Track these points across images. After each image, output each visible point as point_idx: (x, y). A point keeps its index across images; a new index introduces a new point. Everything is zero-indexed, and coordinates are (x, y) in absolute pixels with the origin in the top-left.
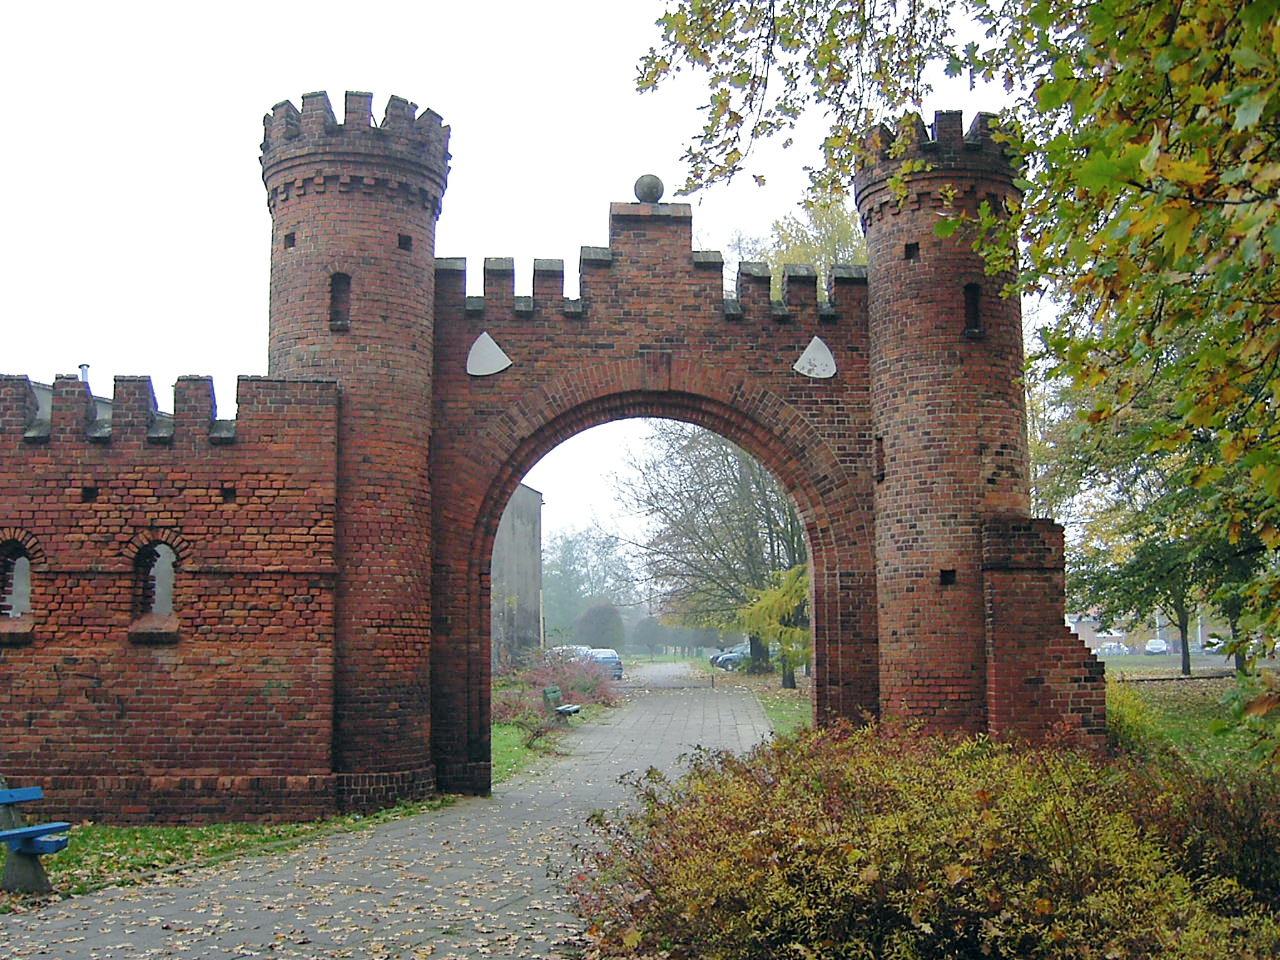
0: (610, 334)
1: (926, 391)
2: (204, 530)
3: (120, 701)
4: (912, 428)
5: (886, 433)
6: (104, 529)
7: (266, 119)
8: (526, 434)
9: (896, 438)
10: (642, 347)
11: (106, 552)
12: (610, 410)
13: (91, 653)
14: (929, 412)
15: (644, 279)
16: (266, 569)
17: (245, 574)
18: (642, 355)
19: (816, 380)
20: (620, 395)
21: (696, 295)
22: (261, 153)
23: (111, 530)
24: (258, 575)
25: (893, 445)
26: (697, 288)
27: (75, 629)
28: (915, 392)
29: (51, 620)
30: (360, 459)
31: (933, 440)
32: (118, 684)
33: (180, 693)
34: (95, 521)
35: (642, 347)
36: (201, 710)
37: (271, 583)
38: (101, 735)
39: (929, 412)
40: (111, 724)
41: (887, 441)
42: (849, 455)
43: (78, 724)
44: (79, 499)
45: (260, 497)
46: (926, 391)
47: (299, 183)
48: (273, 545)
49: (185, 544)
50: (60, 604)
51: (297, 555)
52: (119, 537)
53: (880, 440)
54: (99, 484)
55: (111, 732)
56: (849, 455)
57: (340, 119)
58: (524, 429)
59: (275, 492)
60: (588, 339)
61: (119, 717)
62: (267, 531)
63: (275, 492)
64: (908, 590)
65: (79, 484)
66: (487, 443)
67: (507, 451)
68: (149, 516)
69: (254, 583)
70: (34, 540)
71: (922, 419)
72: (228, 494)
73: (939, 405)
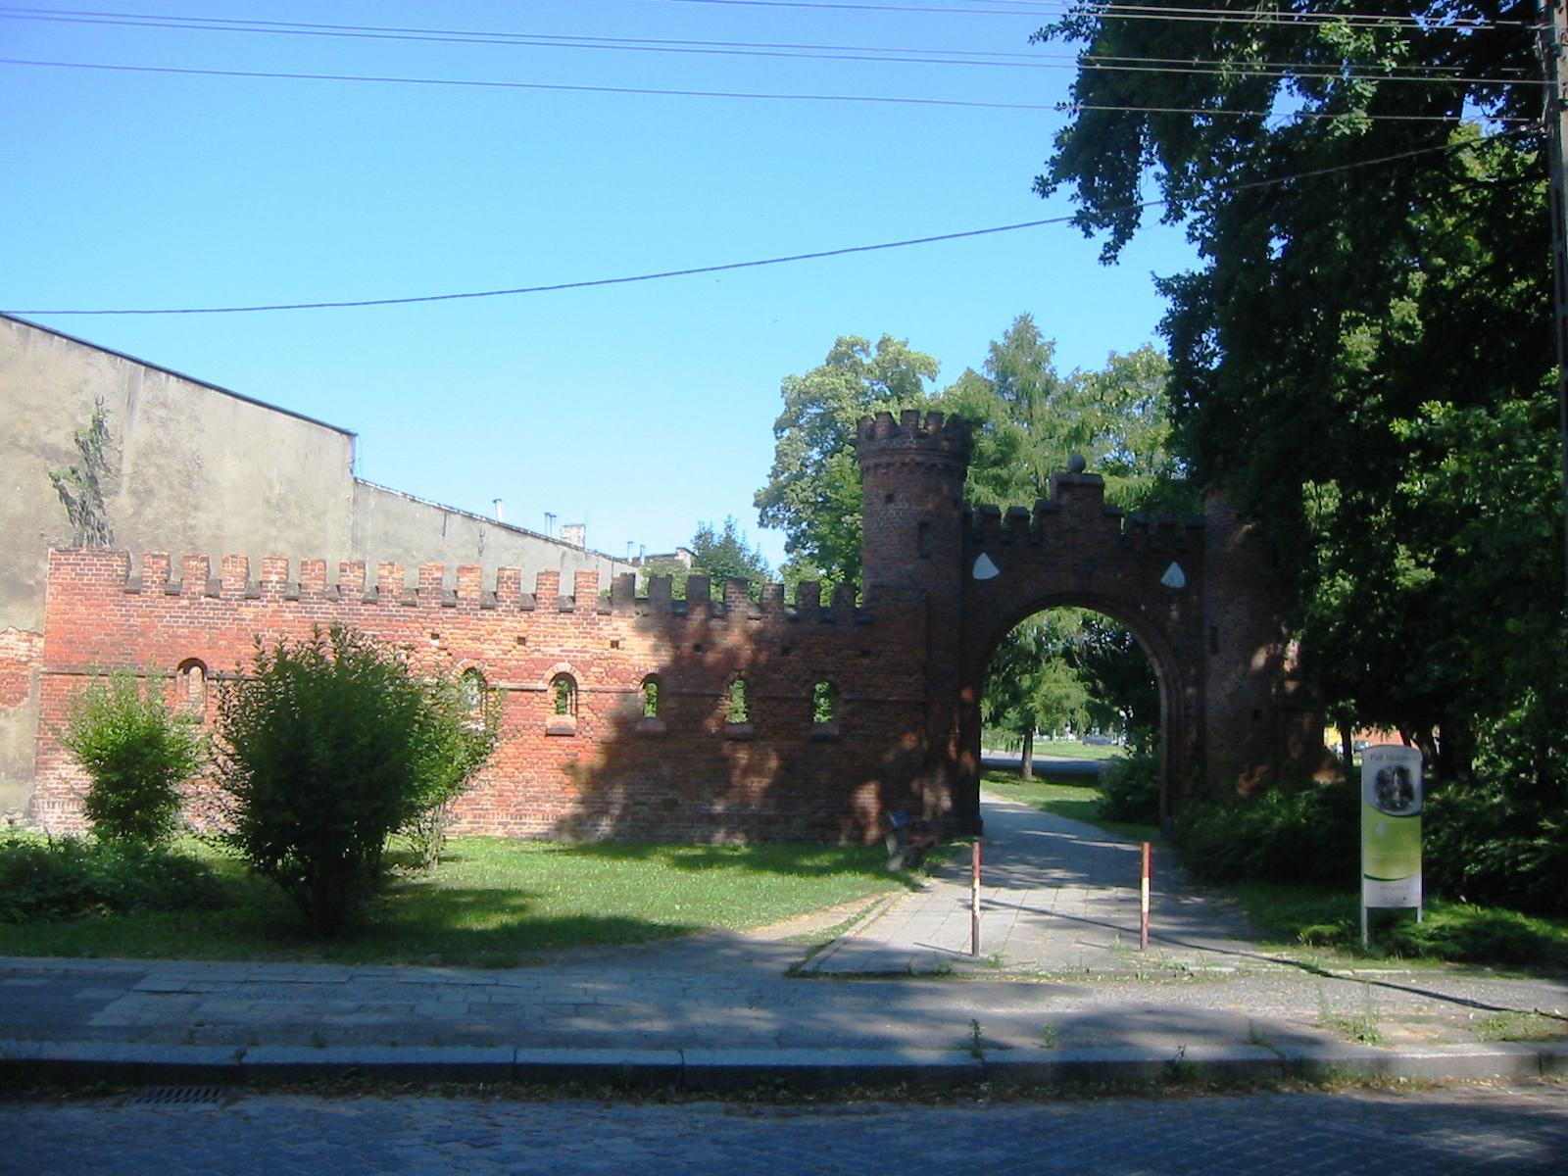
11: (796, 686)
16: (890, 699)
72: (865, 653)
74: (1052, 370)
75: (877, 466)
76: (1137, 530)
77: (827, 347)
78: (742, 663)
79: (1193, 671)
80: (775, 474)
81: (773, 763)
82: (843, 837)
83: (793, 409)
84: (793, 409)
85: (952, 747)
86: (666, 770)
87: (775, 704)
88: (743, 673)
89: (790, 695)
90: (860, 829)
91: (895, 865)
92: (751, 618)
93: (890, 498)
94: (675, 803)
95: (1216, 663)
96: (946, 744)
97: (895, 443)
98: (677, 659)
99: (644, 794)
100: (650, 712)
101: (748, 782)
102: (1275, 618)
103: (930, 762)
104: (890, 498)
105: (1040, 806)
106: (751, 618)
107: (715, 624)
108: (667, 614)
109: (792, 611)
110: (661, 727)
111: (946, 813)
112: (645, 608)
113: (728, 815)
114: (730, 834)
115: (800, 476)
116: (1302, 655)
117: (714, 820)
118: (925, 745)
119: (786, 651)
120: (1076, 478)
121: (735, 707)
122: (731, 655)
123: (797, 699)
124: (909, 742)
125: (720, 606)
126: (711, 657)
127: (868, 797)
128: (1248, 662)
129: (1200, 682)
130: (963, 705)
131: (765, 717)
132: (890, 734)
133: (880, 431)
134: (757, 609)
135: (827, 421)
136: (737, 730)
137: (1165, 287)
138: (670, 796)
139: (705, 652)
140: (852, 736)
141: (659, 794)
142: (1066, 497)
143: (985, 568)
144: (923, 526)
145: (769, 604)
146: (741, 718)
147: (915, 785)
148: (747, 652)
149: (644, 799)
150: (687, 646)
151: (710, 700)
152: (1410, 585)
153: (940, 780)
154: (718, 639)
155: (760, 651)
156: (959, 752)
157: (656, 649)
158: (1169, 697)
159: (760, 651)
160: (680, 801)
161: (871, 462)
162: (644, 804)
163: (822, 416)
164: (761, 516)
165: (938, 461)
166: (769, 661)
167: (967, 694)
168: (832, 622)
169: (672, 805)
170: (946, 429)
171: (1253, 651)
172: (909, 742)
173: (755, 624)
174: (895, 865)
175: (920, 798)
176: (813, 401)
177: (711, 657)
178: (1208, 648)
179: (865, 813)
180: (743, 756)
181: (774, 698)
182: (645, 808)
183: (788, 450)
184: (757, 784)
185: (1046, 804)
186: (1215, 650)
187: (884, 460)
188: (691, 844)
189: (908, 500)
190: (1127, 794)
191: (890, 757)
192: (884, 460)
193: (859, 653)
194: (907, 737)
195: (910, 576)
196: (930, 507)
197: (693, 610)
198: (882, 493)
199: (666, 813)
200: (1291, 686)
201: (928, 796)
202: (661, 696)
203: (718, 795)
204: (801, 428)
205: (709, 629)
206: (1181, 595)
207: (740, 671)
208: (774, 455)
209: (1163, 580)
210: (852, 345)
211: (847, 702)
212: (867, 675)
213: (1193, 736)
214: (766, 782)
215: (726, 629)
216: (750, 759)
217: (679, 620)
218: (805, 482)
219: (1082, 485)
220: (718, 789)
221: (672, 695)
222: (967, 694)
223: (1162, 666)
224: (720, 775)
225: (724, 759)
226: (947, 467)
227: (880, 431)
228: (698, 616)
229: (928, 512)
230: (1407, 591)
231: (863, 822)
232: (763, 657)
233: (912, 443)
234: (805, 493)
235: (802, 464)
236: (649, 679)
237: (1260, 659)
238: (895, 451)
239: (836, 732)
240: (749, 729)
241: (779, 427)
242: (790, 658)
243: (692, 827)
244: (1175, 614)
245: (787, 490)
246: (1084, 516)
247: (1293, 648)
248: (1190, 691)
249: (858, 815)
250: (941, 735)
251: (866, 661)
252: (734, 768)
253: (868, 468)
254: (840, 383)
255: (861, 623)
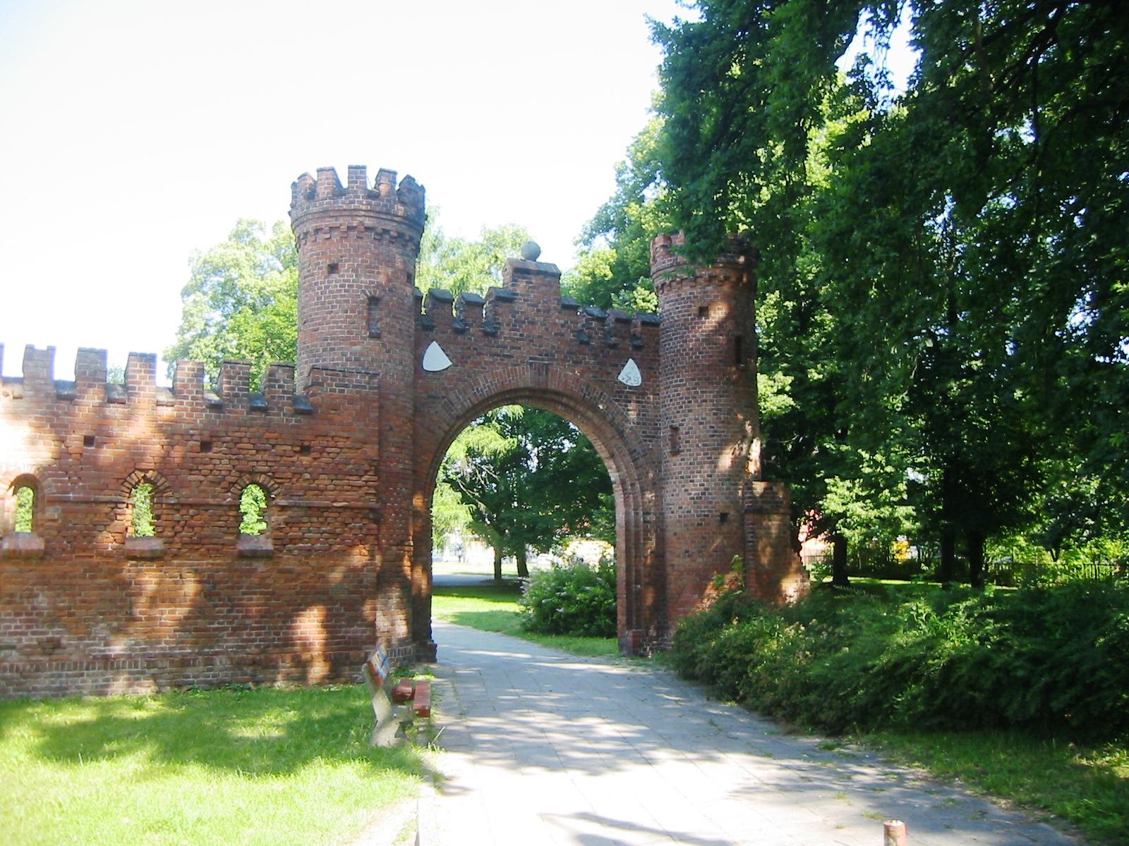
0: (512, 348)
1: (711, 401)
2: (289, 475)
3: (230, 600)
4: (702, 423)
5: (680, 425)
6: (217, 473)
7: (422, 188)
8: (461, 412)
9: (691, 428)
10: (531, 358)
11: (218, 489)
12: (510, 399)
13: (207, 564)
14: (714, 414)
15: (531, 313)
16: (335, 504)
17: (318, 508)
18: (531, 364)
19: (631, 387)
20: (516, 390)
21: (563, 326)
22: (290, 209)
23: (223, 473)
24: (327, 508)
25: (687, 433)
26: (562, 322)
27: (196, 547)
28: (705, 401)
29: (177, 539)
30: (388, 428)
31: (716, 432)
32: (228, 588)
33: (273, 593)
34: (210, 467)
35: (531, 358)
36: (288, 605)
37: (337, 514)
38: (216, 625)
39: (714, 414)
40: (223, 617)
41: (682, 430)
42: (648, 437)
43: (199, 618)
44: (199, 449)
45: (329, 453)
46: (711, 401)
47: (344, 228)
48: (338, 488)
49: (276, 486)
50: (183, 527)
51: (355, 495)
52: (230, 479)
53: (675, 429)
54: (214, 439)
55: (222, 623)
56: (648, 437)
57: (345, 184)
58: (458, 409)
59: (339, 450)
60: (498, 350)
61: (229, 611)
62: (333, 477)
63: (339, 450)
64: (698, 525)
65: (199, 438)
66: (435, 418)
67: (448, 425)
68: (250, 464)
69: (325, 514)
70: (163, 479)
71: (708, 418)
72: (305, 450)
73: (720, 410)
74: (439, 228)
75: (317, 230)
76: (594, 324)
77: (232, 227)
78: (150, 461)
79: (651, 475)
80: (182, 331)
81: (190, 587)
82: (279, 677)
83: (198, 277)
84: (198, 277)
85: (407, 563)
86: (43, 601)
87: (191, 512)
88: (150, 474)
89: (211, 501)
90: (302, 665)
91: (386, 737)
92: (158, 404)
93: (333, 268)
94: (56, 645)
95: (676, 465)
96: (401, 559)
97: (341, 203)
98: (61, 456)
99: (11, 634)
100: (24, 527)
101: (155, 612)
102: (740, 417)
103: (387, 578)
104: (333, 268)
105: (450, 619)
106: (158, 404)
107: (114, 411)
108: (48, 396)
109: (214, 398)
110: (38, 544)
111: (402, 642)
112: (17, 390)
113: (130, 656)
114: (134, 680)
115: (204, 334)
116: (764, 455)
117: (108, 663)
118: (378, 559)
119: (206, 446)
120: (531, 265)
121: (138, 518)
122: (134, 456)
123: (220, 505)
124: (359, 557)
125: (119, 388)
126: (107, 454)
127: (310, 626)
128: (714, 463)
129: (657, 485)
130: (416, 514)
131: (178, 528)
132: (336, 547)
133: (323, 191)
134: (171, 395)
135: (228, 288)
136: (141, 546)
137: (661, 33)
138: (50, 635)
139: (100, 445)
140: (290, 551)
141: (33, 633)
142: (522, 284)
143: (436, 359)
144: (373, 301)
145: (185, 386)
146: (146, 529)
147: (367, 609)
148: (155, 448)
149: (13, 640)
150: (75, 441)
151: (106, 509)
152: (775, 408)
153: (395, 600)
154: (116, 430)
155: (172, 445)
156: (412, 567)
157: (33, 442)
158: (626, 504)
159: (172, 445)
160: (64, 642)
161: (310, 227)
162: (13, 648)
163: (223, 285)
164: (168, 370)
165: (390, 226)
166: (184, 457)
167: (418, 502)
168: (264, 410)
169: (54, 645)
170: (399, 192)
171: (719, 450)
172: (359, 557)
173: (167, 412)
174: (386, 737)
175: (373, 625)
176: (217, 271)
177: (107, 454)
178: (667, 450)
179: (306, 647)
180: (150, 579)
181: (191, 506)
182: (14, 653)
183: (194, 311)
184: (170, 616)
185: (455, 616)
186: (675, 452)
187: (326, 223)
188: (78, 701)
189: (355, 270)
190: (559, 606)
191: (336, 575)
192: (326, 223)
193: (298, 449)
194: (356, 551)
195: (356, 360)
196: (382, 279)
197: (85, 392)
198: (324, 263)
199: (45, 659)
200: (759, 487)
201: (382, 623)
202: (37, 505)
203: (118, 631)
204: (205, 294)
205: (105, 417)
206: (639, 392)
207: (146, 471)
208: (182, 315)
209: (620, 378)
210: (251, 224)
211: (283, 508)
212: (308, 476)
213: (652, 544)
214: (181, 612)
215: (128, 417)
216: (159, 584)
217: (64, 404)
218: (208, 340)
219: (538, 273)
220: (115, 624)
221: (52, 502)
222: (418, 502)
223: (618, 469)
224: (119, 605)
225: (125, 585)
226: (401, 235)
227: (323, 191)
228: (91, 400)
229: (379, 285)
230: (772, 413)
231: (306, 656)
232: (177, 454)
233: (362, 203)
234: (208, 349)
235: (206, 325)
236: (21, 482)
237: (726, 461)
238: (340, 213)
239: (269, 546)
240: (158, 545)
241: (186, 292)
242: (210, 454)
243: (82, 675)
244: (633, 415)
245: (192, 346)
246: (540, 306)
247: (756, 449)
248: (649, 495)
249: (297, 648)
250: (394, 548)
251: (306, 460)
252: (140, 594)
253: (306, 234)
254: (241, 255)
255: (299, 412)
